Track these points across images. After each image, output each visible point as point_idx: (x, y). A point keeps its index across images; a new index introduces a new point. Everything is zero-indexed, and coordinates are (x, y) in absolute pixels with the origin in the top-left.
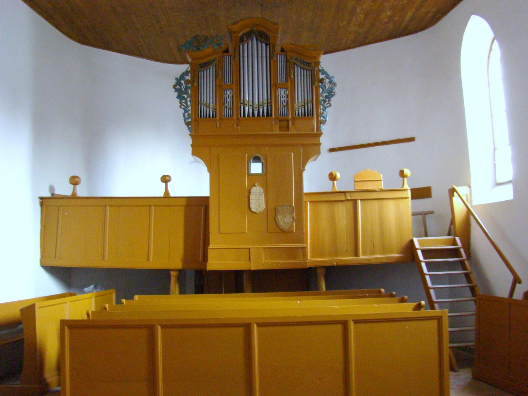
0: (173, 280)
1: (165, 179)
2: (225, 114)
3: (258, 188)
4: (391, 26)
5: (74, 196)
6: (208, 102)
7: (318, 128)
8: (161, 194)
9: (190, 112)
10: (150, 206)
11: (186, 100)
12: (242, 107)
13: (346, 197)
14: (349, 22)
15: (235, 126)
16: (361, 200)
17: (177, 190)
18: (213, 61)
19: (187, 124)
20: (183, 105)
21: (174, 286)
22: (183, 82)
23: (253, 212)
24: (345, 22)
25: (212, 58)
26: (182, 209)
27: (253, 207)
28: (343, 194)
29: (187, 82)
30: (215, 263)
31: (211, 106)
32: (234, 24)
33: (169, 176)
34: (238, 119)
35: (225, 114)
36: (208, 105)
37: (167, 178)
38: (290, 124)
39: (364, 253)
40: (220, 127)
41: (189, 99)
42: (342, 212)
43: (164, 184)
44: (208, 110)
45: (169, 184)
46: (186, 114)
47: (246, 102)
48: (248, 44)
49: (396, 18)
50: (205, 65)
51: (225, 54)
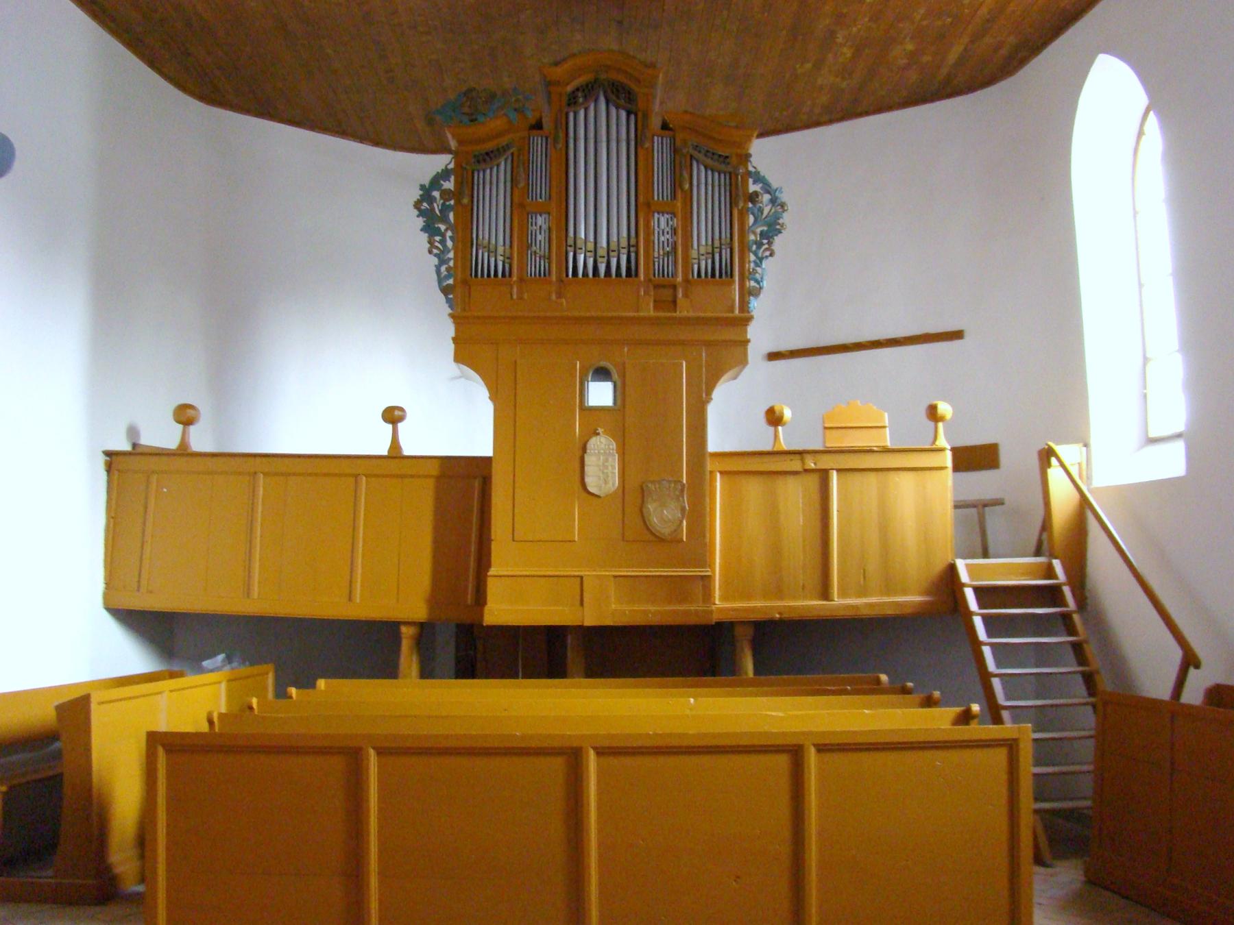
0: (406, 645)
1: (393, 416)
2: (531, 269)
3: (603, 440)
4: (913, 76)
5: (183, 451)
6: (493, 241)
7: (744, 306)
8: (382, 449)
9: (451, 264)
10: (356, 476)
11: (443, 235)
12: (571, 254)
13: (803, 463)
14: (818, 65)
15: (554, 297)
16: (838, 470)
17: (427, 438)
18: (505, 149)
19: (445, 291)
20: (437, 248)
21: (409, 661)
22: (436, 194)
23: (592, 494)
24: (809, 66)
25: (504, 141)
26: (431, 483)
27: (592, 483)
28: (798, 457)
29: (446, 194)
30: (501, 609)
31: (500, 250)
32: (557, 64)
33: (401, 409)
34: (560, 281)
35: (531, 269)
36: (492, 248)
37: (397, 413)
38: (680, 295)
39: (843, 593)
40: (520, 298)
41: (449, 234)
42: (794, 497)
43: (390, 426)
44: (492, 260)
45: (400, 425)
46: (443, 268)
47: (580, 244)
48: (586, 110)
49: (926, 58)
50: (488, 157)
51: (535, 132)
